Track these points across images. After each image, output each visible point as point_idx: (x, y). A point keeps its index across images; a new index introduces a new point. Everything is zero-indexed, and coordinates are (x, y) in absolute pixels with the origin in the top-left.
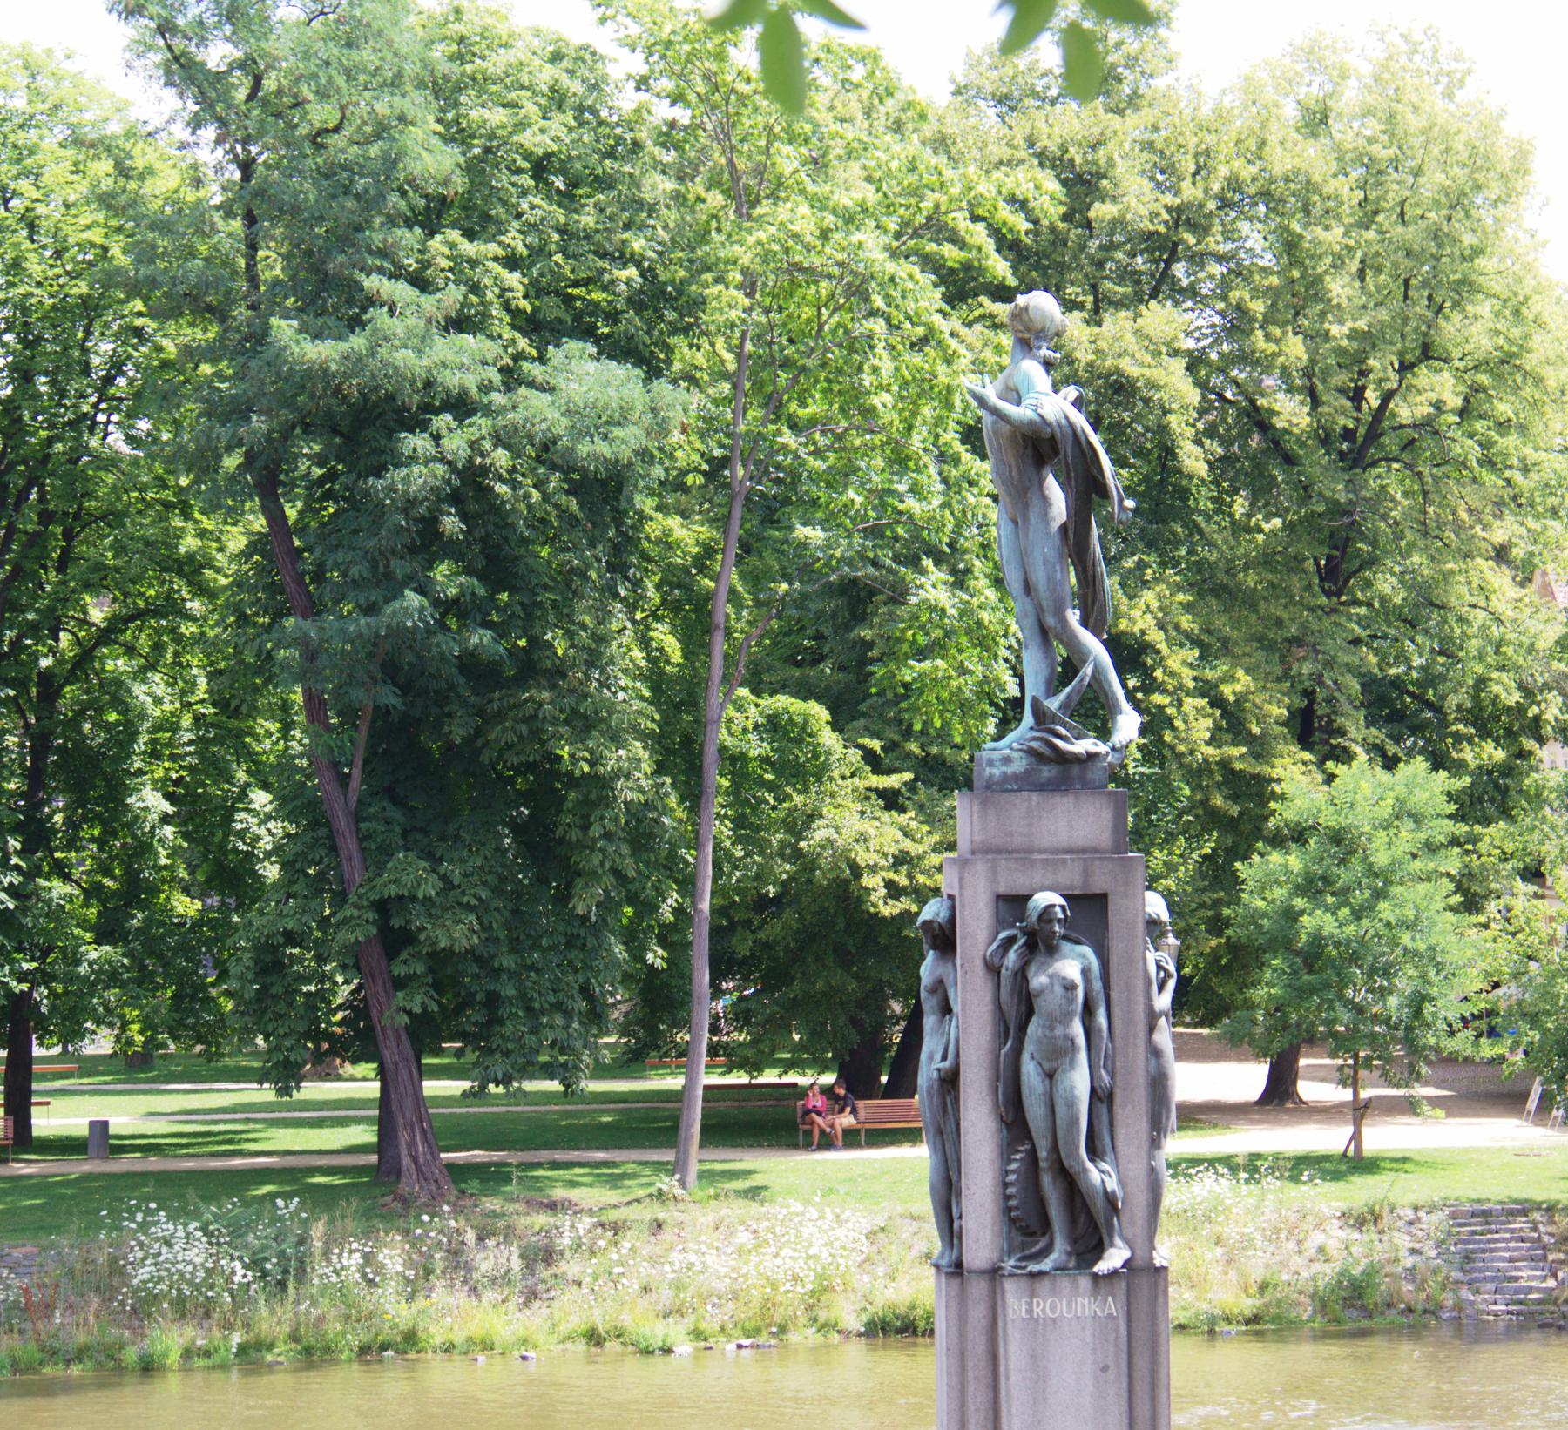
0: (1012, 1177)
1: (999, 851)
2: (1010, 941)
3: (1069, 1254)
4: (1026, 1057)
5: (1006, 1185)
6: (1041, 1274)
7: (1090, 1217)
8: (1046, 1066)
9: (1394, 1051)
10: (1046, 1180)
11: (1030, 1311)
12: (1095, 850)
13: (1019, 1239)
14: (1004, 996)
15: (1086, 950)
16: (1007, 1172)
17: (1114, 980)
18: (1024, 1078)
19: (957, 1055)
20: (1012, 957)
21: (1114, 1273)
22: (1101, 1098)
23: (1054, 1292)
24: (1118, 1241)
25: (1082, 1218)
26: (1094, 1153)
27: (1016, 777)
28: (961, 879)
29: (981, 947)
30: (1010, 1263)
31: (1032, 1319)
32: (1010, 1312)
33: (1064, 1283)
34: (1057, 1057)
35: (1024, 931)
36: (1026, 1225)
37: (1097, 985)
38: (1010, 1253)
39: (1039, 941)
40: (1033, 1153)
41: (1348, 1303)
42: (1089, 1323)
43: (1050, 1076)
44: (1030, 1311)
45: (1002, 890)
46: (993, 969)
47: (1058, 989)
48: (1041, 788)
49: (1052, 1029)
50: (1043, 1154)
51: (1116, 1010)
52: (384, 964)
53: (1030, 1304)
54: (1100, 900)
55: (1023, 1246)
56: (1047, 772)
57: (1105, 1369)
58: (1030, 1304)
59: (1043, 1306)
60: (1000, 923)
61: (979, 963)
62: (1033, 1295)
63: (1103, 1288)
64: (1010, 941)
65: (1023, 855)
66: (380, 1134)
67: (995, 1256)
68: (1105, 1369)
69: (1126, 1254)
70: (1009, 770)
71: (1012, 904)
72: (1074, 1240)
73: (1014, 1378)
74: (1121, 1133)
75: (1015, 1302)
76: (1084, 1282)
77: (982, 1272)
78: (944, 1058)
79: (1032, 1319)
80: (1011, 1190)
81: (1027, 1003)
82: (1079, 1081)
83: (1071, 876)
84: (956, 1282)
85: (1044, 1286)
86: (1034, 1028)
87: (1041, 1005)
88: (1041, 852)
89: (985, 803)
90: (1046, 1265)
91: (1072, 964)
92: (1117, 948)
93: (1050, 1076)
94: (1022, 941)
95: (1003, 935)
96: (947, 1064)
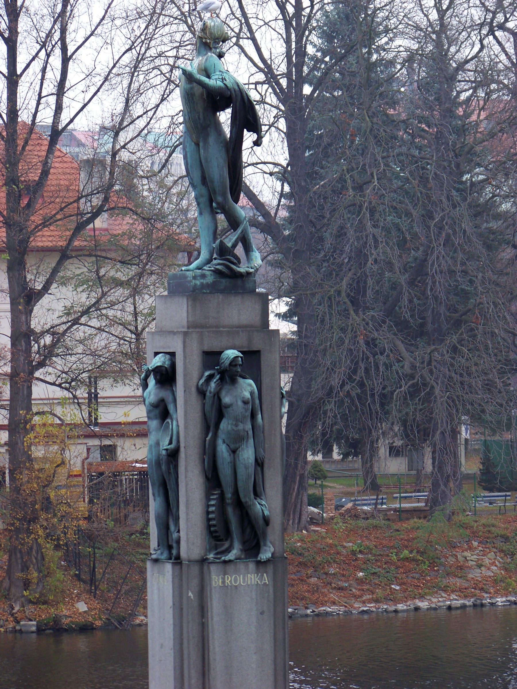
0: (212, 509)
1: (202, 327)
2: (210, 377)
3: (241, 550)
4: (220, 442)
5: (208, 513)
6: (230, 561)
7: (253, 528)
8: (232, 446)
10: (230, 510)
11: (224, 582)
12: (252, 326)
13: (214, 543)
14: (207, 407)
15: (251, 382)
16: (208, 506)
17: (264, 398)
18: (219, 454)
19: (178, 441)
20: (213, 385)
21: (268, 561)
22: (259, 463)
23: (237, 572)
24: (268, 543)
25: (248, 530)
26: (257, 495)
27: (208, 285)
28: (184, 342)
29: (195, 381)
30: (211, 556)
31: (224, 587)
33: (241, 567)
34: (236, 443)
36: (217, 534)
37: (257, 402)
38: (210, 551)
39: (229, 376)
40: (222, 496)
41: (217, 539)
42: (254, 587)
43: (234, 452)
44: (224, 582)
45: (206, 349)
46: (202, 393)
47: (240, 403)
48: (222, 291)
49: (237, 426)
50: (229, 495)
51: (265, 415)
53: (223, 579)
54: (257, 353)
55: (216, 547)
56: (224, 282)
57: (262, 613)
58: (223, 579)
59: (229, 580)
60: (206, 366)
61: (194, 389)
64: (210, 377)
65: (216, 329)
66: (298, 327)
67: (203, 552)
68: (262, 613)
69: (272, 549)
70: (204, 281)
71: (211, 357)
72: (244, 543)
73: (215, 619)
74: (267, 485)
75: (216, 579)
76: (252, 566)
78: (170, 443)
79: (224, 587)
80: (211, 516)
81: (221, 411)
82: (248, 454)
83: (242, 340)
84: (178, 567)
85: (231, 568)
86: (224, 425)
87: (229, 413)
88: (224, 327)
89: (194, 300)
90: (231, 556)
91: (247, 387)
92: (266, 381)
94: (218, 377)
95: (207, 374)
96: (172, 446)
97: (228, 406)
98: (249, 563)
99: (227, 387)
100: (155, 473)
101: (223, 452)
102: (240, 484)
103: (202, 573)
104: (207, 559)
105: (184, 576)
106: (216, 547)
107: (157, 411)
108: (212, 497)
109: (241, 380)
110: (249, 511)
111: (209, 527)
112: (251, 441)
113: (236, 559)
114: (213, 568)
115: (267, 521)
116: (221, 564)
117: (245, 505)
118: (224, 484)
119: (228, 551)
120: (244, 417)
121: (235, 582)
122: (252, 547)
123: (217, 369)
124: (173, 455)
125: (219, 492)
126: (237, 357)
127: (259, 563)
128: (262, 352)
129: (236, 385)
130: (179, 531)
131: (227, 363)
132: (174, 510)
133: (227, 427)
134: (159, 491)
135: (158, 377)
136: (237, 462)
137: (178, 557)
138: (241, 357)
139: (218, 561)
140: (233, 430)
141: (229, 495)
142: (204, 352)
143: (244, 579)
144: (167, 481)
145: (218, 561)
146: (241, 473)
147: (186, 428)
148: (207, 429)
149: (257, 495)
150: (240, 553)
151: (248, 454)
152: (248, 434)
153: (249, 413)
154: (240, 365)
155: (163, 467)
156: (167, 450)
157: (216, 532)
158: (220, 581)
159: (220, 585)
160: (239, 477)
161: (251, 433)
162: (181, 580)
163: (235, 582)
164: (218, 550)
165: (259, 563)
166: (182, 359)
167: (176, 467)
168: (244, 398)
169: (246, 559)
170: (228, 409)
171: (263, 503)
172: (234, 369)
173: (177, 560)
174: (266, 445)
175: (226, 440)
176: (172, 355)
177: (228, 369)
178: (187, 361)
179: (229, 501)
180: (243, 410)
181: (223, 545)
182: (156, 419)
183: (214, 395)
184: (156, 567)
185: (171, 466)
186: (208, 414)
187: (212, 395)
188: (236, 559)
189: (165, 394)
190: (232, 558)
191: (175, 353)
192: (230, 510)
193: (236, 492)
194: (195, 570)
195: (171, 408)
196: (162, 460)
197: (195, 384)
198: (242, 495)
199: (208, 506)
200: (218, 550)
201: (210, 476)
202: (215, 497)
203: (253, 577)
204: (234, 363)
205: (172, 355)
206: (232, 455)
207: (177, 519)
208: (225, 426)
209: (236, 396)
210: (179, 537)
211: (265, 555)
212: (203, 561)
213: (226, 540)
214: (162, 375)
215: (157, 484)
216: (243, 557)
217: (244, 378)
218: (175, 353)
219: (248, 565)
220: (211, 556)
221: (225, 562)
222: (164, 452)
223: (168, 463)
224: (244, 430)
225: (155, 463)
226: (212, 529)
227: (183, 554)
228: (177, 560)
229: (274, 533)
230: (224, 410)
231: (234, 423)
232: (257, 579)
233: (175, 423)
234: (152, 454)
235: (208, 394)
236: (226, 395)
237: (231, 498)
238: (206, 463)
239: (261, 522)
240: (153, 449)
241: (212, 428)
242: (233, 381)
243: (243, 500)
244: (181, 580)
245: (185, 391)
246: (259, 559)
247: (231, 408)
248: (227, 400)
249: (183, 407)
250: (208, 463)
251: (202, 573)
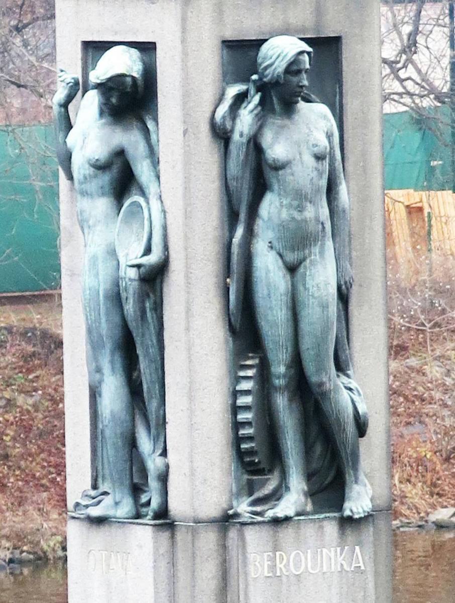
2: (241, 99)
5: (235, 409)
6: (287, 519)
8: (291, 257)
9: (5, 328)
10: (281, 402)
11: (273, 567)
19: (166, 248)
21: (367, 518)
24: (362, 477)
25: (318, 449)
32: (251, 569)
33: (309, 531)
34: (297, 247)
35: (262, 87)
36: (255, 459)
38: (238, 495)
40: (264, 369)
44: (273, 567)
45: (230, 35)
46: (222, 135)
49: (301, 209)
50: (280, 369)
52: (61, 136)
54: (335, 41)
55: (250, 488)
62: (276, 549)
63: (350, 536)
64: (241, 99)
71: (241, 53)
72: (309, 476)
76: (331, 529)
77: (213, 521)
78: (148, 251)
80: (242, 416)
82: (322, 276)
84: (166, 535)
85: (287, 533)
86: (270, 206)
90: (287, 506)
91: (314, 118)
93: (292, 269)
94: (257, 99)
95: (233, 90)
96: (154, 258)
97: (278, 167)
98: (325, 523)
99: (275, 122)
100: (103, 320)
101: (268, 272)
102: (307, 343)
103: (224, 547)
104: (236, 515)
105: (180, 555)
106: (250, 488)
107: (106, 179)
108: (242, 374)
109: (302, 105)
110: (326, 406)
111: (238, 440)
112: (329, 244)
113: (298, 514)
114: (252, 535)
115: (361, 427)
116: (151, 527)
117: (316, 390)
118: (269, 344)
119: (275, 496)
120: (318, 190)
121: (297, 567)
122: (329, 487)
123: (254, 81)
124: (154, 278)
125: (257, 361)
126: (302, 53)
127: (347, 523)
128: (344, 41)
129: (296, 117)
130: (164, 453)
131: (280, 67)
132: (153, 406)
133: (279, 213)
134: (112, 362)
135: (114, 100)
136: (302, 295)
137: (163, 513)
138: (309, 53)
139: (259, 519)
140: (293, 218)
141: (280, 369)
142: (224, 42)
143: (314, 558)
144: (138, 340)
145: (259, 519)
146: (311, 316)
147: (187, 215)
148: (232, 217)
149: (341, 367)
150: (302, 498)
151: (322, 276)
152: (324, 228)
153: (324, 183)
154: (306, 71)
155: (130, 308)
156: (139, 266)
157: (251, 452)
158: (267, 563)
159: (266, 574)
160: (305, 327)
161: (328, 226)
162: (173, 563)
163: (297, 567)
164: (258, 494)
165: (347, 523)
166: (178, 59)
167: (158, 307)
168: (315, 145)
169: (315, 512)
170: (280, 172)
171: (353, 384)
172: (295, 79)
173: (164, 518)
174: (354, 254)
175: (275, 244)
176: (147, 48)
177: (282, 81)
178: (190, 64)
179: (279, 382)
180: (315, 174)
181: (263, 484)
182: (103, 194)
183: (249, 142)
184: (100, 535)
185: (147, 305)
186: (233, 184)
187: (244, 140)
188: (298, 514)
189: (129, 139)
190: (291, 512)
191: (154, 43)
192: (281, 402)
193: (297, 362)
194: (209, 539)
195: (143, 170)
196: (126, 289)
197: (208, 115)
198: (310, 367)
199: (235, 394)
200: (258, 494)
201: (238, 326)
202: (250, 373)
203: (332, 555)
204: (295, 68)
205: (147, 48)
206: (288, 277)
207: (159, 427)
208: (274, 210)
209: (298, 144)
210: (167, 467)
211: (359, 501)
212: (226, 520)
213: (271, 471)
214: (123, 94)
215: (109, 346)
216: (309, 508)
217: (308, 101)
218: (154, 43)
219: (321, 527)
220: (243, 507)
221: (276, 522)
222: (133, 273)
223: (142, 297)
224: (317, 219)
225: (106, 297)
226: (244, 446)
227: (176, 506)
228: (164, 518)
229: (372, 454)
230: (270, 175)
231: (295, 203)
232: (340, 559)
233: (155, 205)
234: (97, 275)
235: (236, 137)
236: (276, 139)
237: (284, 376)
238: (232, 297)
239: (351, 428)
240: (101, 266)
241: (243, 216)
242: (289, 108)
243: (314, 379)
244: (173, 563)
245: (185, 132)
246: (347, 513)
247: (288, 171)
248: (277, 148)
249: (179, 167)
250: (237, 298)
251: (224, 547)
